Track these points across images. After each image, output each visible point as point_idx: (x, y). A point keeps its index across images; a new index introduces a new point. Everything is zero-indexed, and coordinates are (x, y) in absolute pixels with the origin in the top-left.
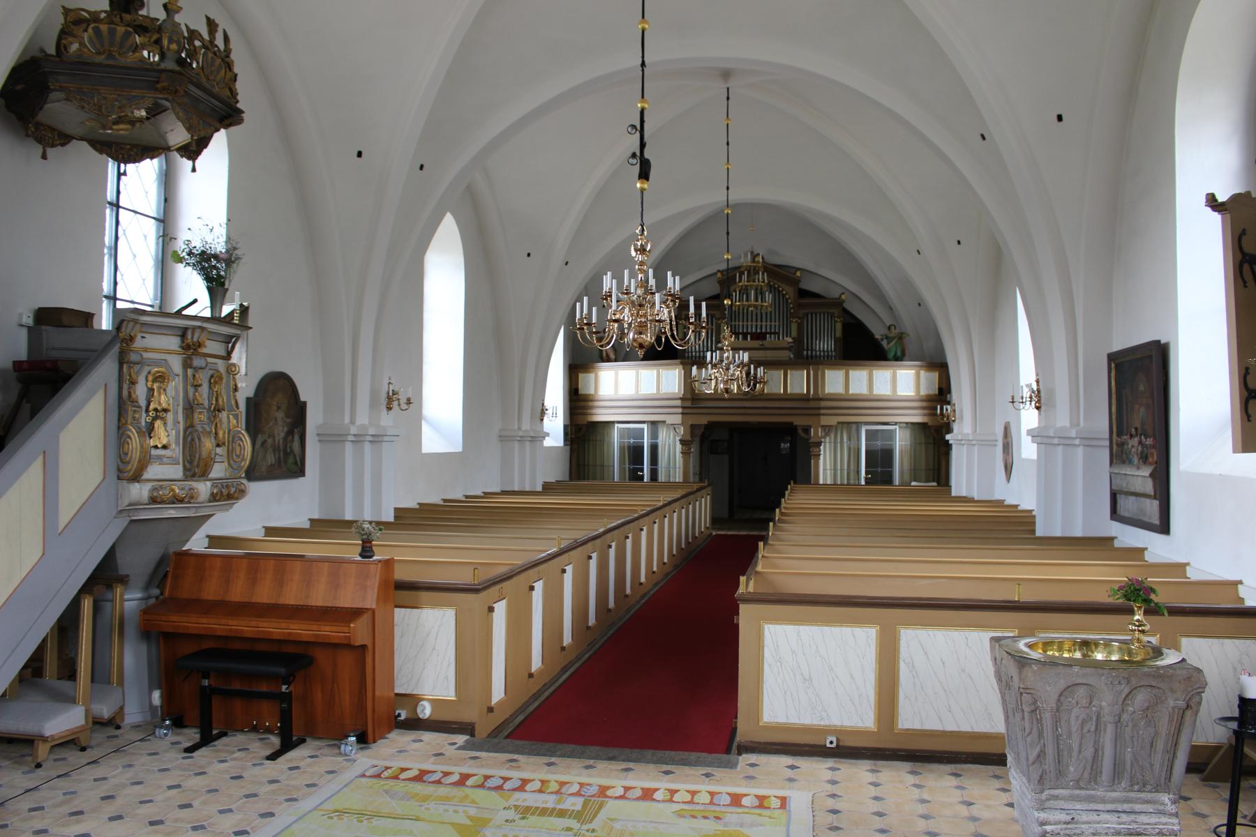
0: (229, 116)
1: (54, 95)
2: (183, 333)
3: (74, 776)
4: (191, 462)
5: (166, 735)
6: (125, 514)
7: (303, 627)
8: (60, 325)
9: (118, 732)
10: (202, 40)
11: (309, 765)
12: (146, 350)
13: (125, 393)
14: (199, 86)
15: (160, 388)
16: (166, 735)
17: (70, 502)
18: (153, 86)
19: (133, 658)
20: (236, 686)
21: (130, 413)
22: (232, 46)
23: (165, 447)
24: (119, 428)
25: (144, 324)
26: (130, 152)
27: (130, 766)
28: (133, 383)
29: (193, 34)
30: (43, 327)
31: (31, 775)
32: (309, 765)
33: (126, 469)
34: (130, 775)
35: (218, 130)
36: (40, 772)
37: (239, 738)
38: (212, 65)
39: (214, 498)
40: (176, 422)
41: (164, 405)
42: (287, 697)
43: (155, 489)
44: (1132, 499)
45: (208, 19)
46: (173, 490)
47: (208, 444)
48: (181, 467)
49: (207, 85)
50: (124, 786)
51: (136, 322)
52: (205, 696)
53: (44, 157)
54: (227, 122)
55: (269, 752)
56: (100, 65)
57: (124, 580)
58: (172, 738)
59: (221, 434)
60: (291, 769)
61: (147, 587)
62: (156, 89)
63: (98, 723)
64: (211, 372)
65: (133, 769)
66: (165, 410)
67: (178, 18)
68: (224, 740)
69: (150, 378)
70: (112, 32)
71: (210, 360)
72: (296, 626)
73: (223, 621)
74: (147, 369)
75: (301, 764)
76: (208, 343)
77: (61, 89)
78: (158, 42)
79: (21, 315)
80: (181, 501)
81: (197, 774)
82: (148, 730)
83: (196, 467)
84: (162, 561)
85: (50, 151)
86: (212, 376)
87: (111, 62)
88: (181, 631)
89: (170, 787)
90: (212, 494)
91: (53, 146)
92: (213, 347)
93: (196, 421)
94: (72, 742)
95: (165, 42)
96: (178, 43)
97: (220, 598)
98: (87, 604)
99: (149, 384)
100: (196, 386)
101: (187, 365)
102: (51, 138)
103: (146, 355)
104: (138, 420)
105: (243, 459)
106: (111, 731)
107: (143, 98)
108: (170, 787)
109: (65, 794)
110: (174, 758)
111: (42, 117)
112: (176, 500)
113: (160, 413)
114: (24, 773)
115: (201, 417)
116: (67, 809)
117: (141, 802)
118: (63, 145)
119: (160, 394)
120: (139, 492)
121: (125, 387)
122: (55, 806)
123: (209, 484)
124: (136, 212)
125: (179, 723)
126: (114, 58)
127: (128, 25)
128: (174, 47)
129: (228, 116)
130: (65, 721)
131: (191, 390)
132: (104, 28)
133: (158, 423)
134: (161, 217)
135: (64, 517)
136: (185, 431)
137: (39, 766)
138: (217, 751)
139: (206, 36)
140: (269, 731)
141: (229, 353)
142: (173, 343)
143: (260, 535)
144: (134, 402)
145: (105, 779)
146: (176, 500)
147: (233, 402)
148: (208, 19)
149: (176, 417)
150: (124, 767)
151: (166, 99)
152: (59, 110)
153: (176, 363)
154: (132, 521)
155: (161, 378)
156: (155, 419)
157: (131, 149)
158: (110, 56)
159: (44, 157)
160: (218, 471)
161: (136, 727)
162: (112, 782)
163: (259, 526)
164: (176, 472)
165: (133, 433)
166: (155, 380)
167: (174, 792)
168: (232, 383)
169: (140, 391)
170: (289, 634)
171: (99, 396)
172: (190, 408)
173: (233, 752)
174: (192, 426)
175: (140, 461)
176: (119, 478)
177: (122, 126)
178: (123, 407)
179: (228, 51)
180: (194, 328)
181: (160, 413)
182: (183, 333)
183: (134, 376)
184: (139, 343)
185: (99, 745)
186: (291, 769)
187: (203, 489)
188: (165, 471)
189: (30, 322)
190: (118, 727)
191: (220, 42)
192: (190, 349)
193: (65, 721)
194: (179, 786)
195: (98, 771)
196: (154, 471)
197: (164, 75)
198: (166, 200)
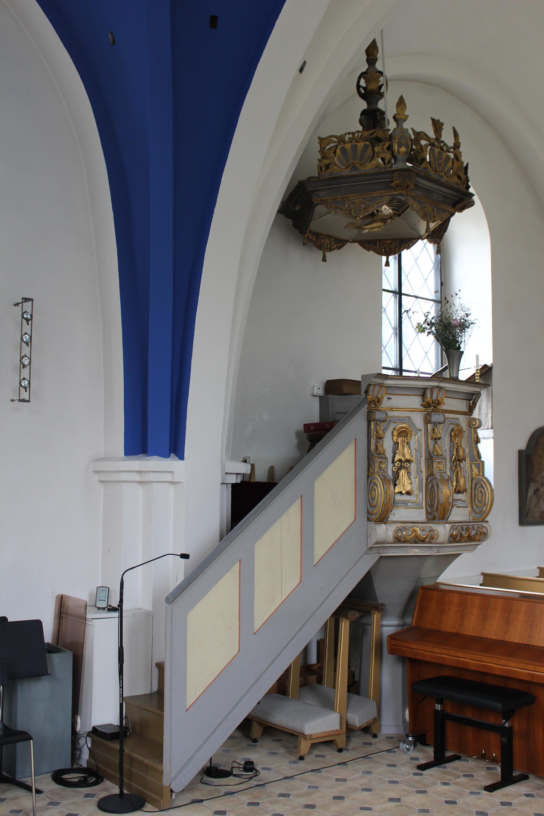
0: (463, 201)
1: (320, 209)
2: (423, 393)
3: (324, 773)
4: (431, 506)
5: (408, 750)
6: (375, 551)
7: (520, 665)
8: (342, 394)
9: (375, 740)
10: (427, 138)
11: (522, 804)
12: (392, 409)
13: (373, 447)
14: (428, 178)
15: (403, 441)
16: (408, 750)
17: (325, 537)
18: (388, 186)
19: (390, 678)
20: (469, 714)
21: (377, 464)
22: (461, 140)
23: (408, 493)
24: (368, 476)
25: (388, 387)
26: (394, 245)
27: (369, 773)
28: (380, 438)
29: (419, 135)
30: (330, 396)
31: (294, 765)
32: (522, 804)
33: (377, 513)
34: (365, 781)
35: (453, 215)
36: (302, 764)
37: (469, 764)
38: (439, 159)
39: (453, 539)
40: (419, 471)
41: (408, 457)
42: (508, 733)
43: (399, 530)
44: (515, 601)
45: (433, 120)
46: (415, 531)
47: (445, 491)
48: (424, 511)
49: (435, 177)
50: (355, 790)
51: (381, 385)
52: (441, 719)
53: (324, 260)
54: (460, 206)
55: (489, 783)
56: (347, 177)
57: (380, 608)
58: (413, 753)
59: (462, 481)
60: (503, 804)
61: (404, 614)
62: (392, 188)
63: (350, 730)
64: (451, 427)
65: (370, 776)
66: (409, 461)
67: (405, 125)
68: (457, 763)
69: (395, 433)
70: (354, 148)
71: (447, 415)
72: (514, 664)
73: (452, 653)
74: (392, 426)
75: (515, 801)
76: (446, 400)
77: (322, 202)
78: (390, 148)
79: (313, 387)
80: (423, 541)
81: (418, 792)
82: (395, 741)
83: (437, 512)
84: (413, 595)
85: (328, 254)
86: (453, 430)
87: (354, 173)
88: (419, 658)
89: (391, 800)
90: (451, 535)
91: (331, 250)
92: (449, 404)
93: (435, 470)
94: (327, 742)
95: (396, 147)
96: (406, 146)
97: (456, 631)
98: (345, 627)
99: (395, 438)
100: (436, 440)
101: (427, 421)
102: (327, 244)
103: (390, 414)
104: (385, 470)
105: (485, 505)
106: (369, 738)
107: (382, 197)
108: (391, 800)
109: (309, 787)
110: (406, 771)
111: (314, 226)
112: (418, 540)
113: (404, 464)
114: (290, 762)
115: (444, 467)
116: (304, 801)
117: (362, 808)
118: (339, 248)
119: (403, 447)
120: (385, 532)
121: (373, 441)
122: (299, 796)
123: (448, 526)
124: (417, 297)
125: (420, 740)
126: (356, 169)
127: (366, 140)
128: (403, 149)
129: (460, 200)
130: (321, 723)
131: (431, 443)
132: (348, 146)
133: (403, 472)
134: (439, 299)
135: (320, 550)
136: (427, 479)
137: (302, 758)
138: (445, 773)
139: (432, 135)
140: (493, 760)
141: (471, 409)
142: (416, 402)
143: (534, 575)
144: (382, 455)
145: (345, 780)
146: (418, 540)
147: (475, 453)
148: (433, 120)
149: (419, 467)
150: (364, 772)
151: (400, 195)
152: (327, 219)
153: (418, 420)
154: (382, 557)
155: (404, 433)
156: (400, 468)
157: (391, 243)
158: (354, 168)
159: (324, 260)
160: (459, 514)
161: (389, 738)
162: (349, 784)
163: (535, 567)
164: (420, 515)
165: (379, 482)
166: (399, 435)
167: (393, 804)
168: (473, 435)
169: (387, 445)
170: (508, 671)
171: (350, 450)
172: (430, 459)
173: (458, 777)
174: (432, 474)
175: (384, 505)
176: (368, 520)
177: (375, 225)
178: (372, 458)
179: (457, 146)
180: (432, 388)
181: (404, 464)
182: (423, 393)
183: (381, 432)
184: (385, 404)
185: (354, 749)
186: (503, 804)
187: (443, 530)
188: (410, 514)
189: (321, 392)
190: (375, 736)
191: (448, 138)
192: (431, 407)
193: (321, 723)
194: (398, 800)
195: (342, 772)
196: (399, 514)
197: (395, 174)
198: (442, 284)
